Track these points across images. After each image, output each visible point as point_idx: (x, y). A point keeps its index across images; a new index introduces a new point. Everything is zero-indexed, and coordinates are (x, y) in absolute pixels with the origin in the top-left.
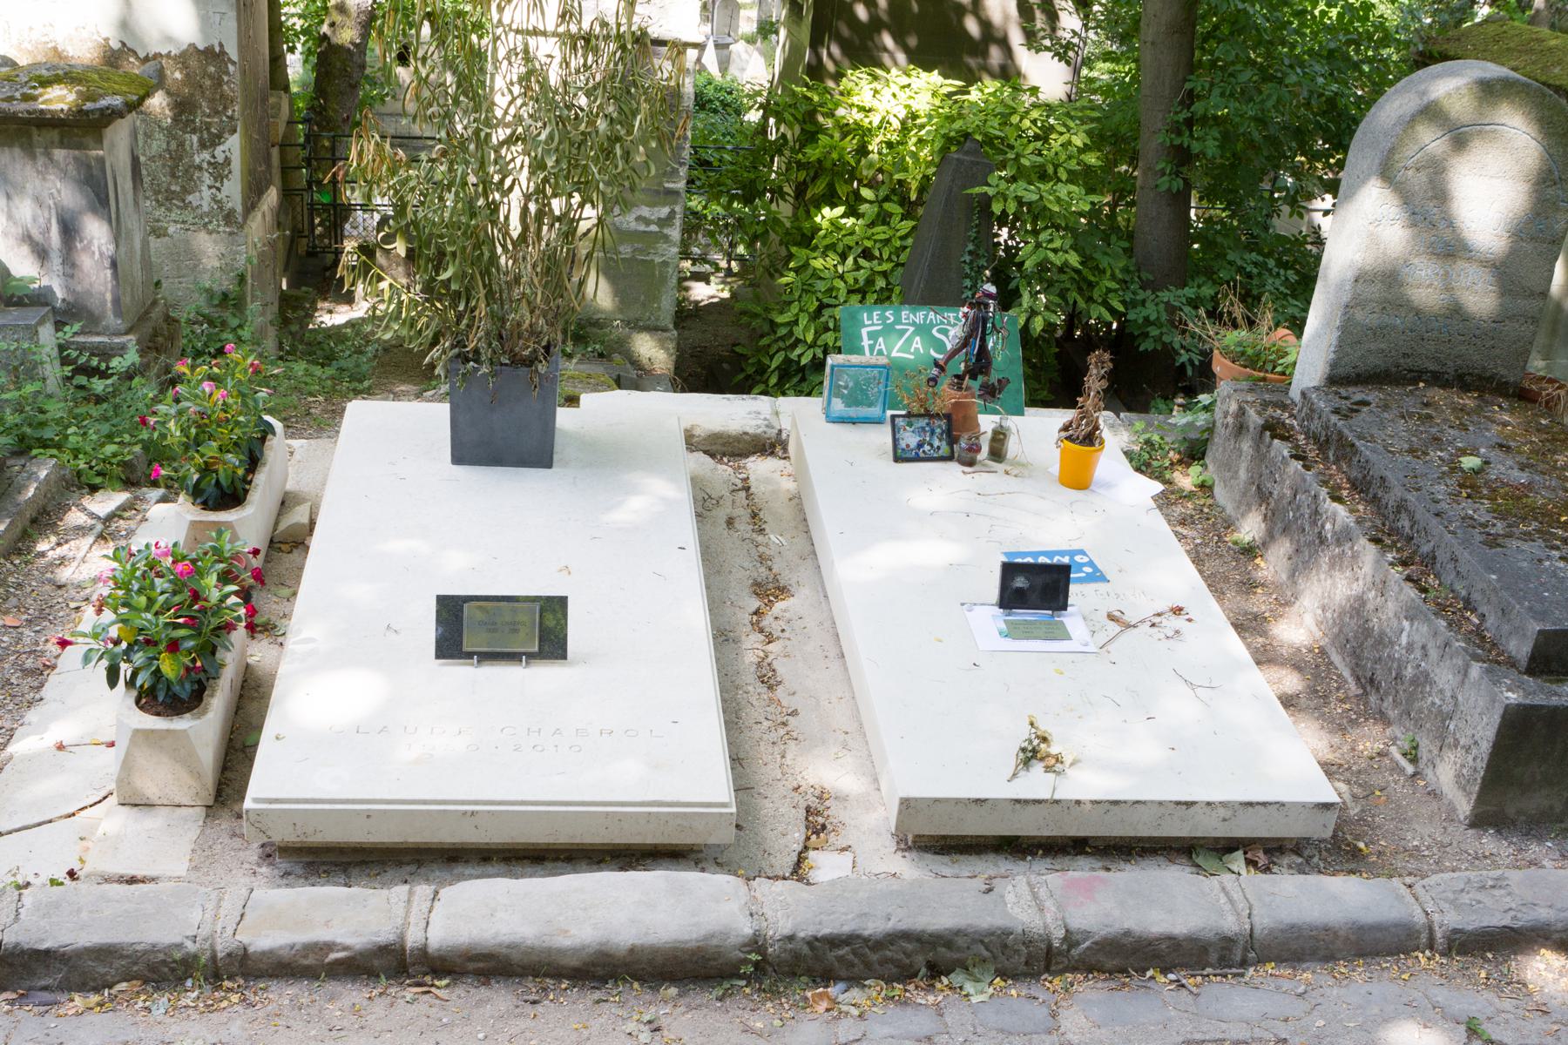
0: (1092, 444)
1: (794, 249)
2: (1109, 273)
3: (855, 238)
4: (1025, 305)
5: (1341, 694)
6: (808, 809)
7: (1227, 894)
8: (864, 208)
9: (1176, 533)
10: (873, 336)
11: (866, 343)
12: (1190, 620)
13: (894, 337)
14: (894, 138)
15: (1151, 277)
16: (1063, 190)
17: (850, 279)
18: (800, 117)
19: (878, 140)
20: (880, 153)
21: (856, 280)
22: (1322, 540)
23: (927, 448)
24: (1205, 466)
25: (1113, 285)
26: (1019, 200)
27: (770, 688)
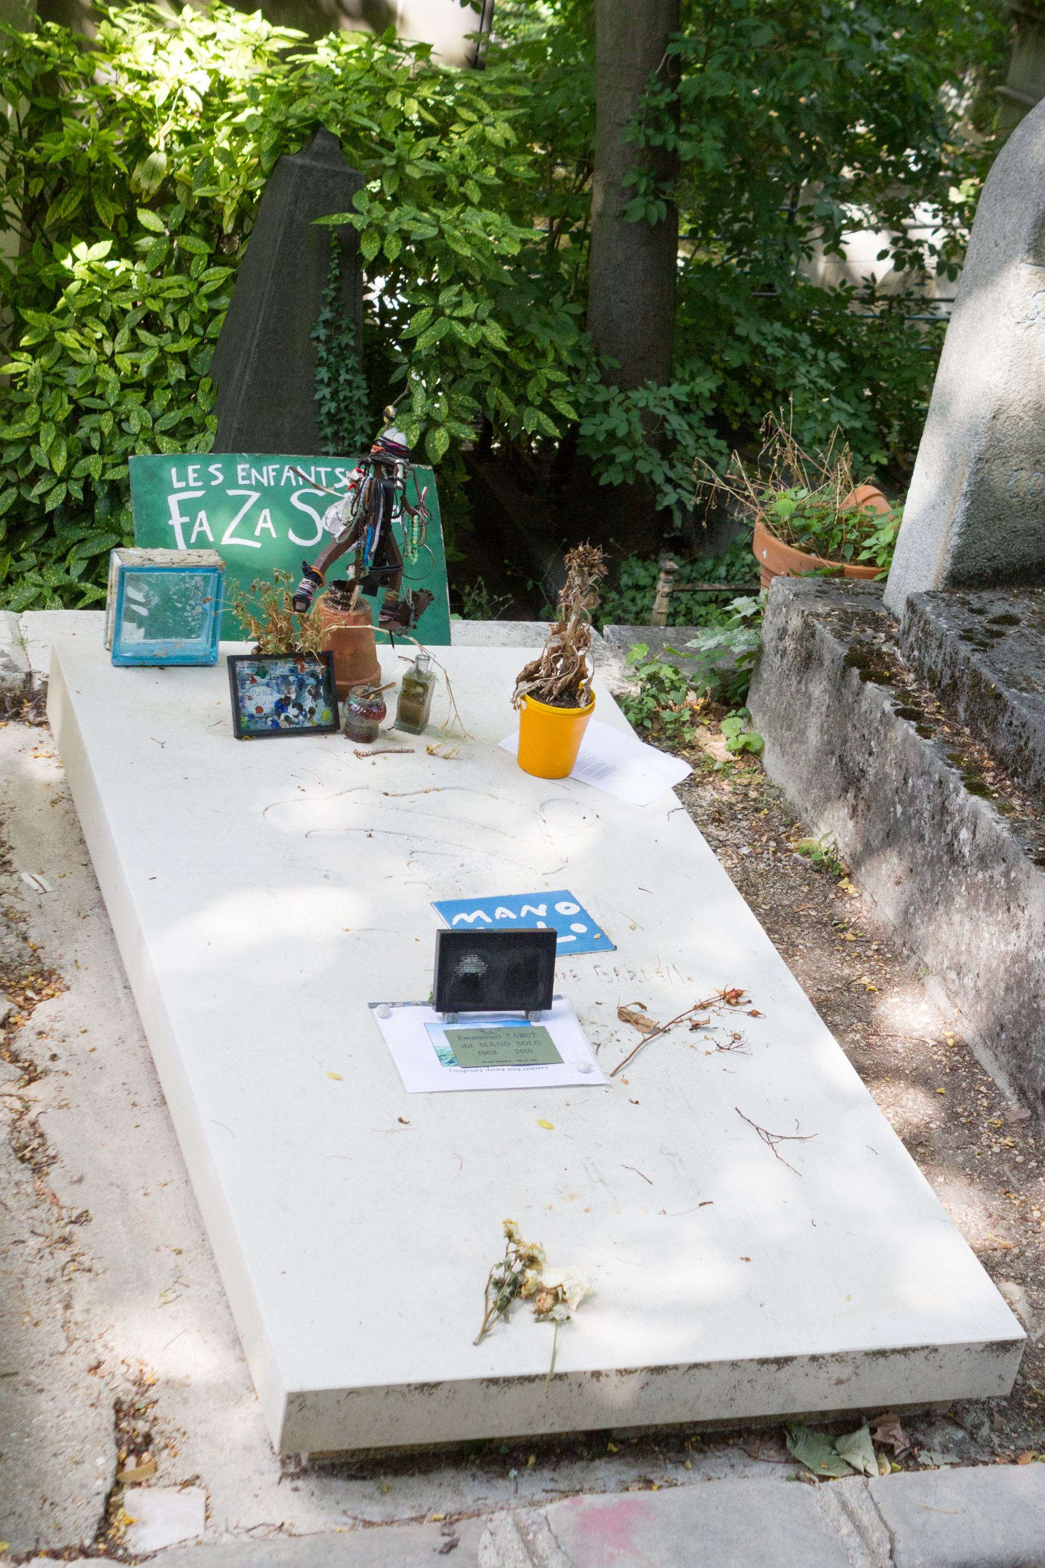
0: (574, 704)
1: (29, 314)
2: (551, 357)
3: (129, 294)
4: (418, 411)
5: (996, 1120)
6: (118, 1407)
7: (851, 1515)
8: (146, 243)
9: (709, 838)
10: (188, 508)
11: (177, 521)
12: (754, 1014)
13: (222, 516)
14: (192, 124)
15: (617, 365)
16: (476, 220)
17: (124, 362)
18: (28, 84)
19: (165, 129)
20: (169, 151)
21: (135, 366)
22: (955, 859)
23: (292, 711)
24: (748, 718)
25: (560, 377)
26: (405, 237)
27: (37, 1170)
